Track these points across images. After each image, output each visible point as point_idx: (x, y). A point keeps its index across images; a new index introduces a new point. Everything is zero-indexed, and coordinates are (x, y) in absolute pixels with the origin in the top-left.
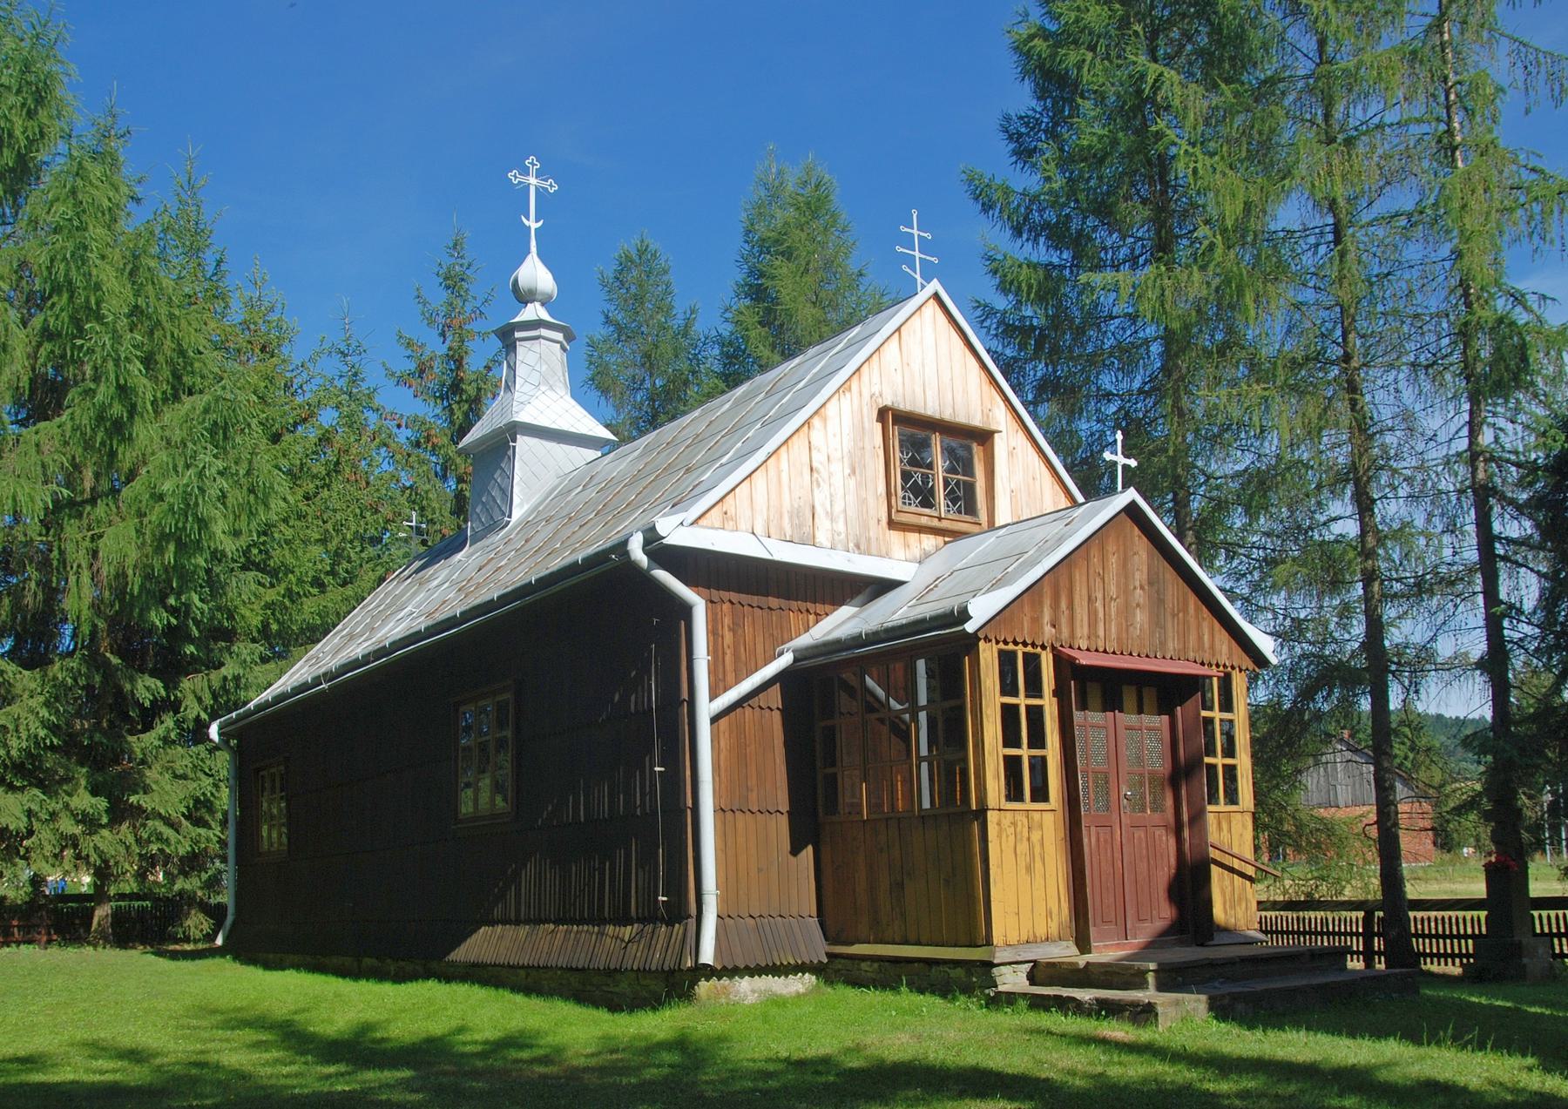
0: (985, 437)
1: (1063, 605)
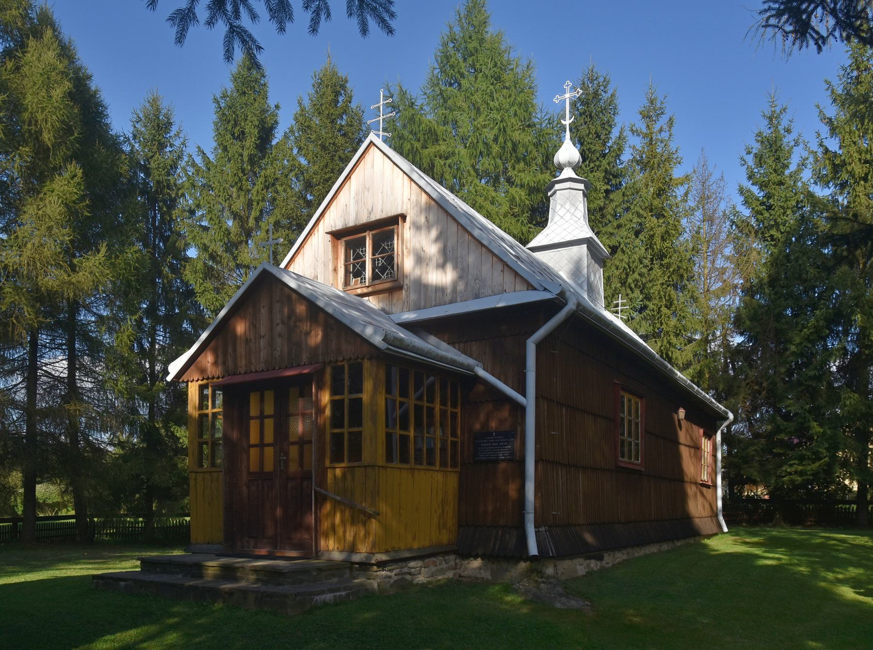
0: (336, 235)
1: (230, 350)
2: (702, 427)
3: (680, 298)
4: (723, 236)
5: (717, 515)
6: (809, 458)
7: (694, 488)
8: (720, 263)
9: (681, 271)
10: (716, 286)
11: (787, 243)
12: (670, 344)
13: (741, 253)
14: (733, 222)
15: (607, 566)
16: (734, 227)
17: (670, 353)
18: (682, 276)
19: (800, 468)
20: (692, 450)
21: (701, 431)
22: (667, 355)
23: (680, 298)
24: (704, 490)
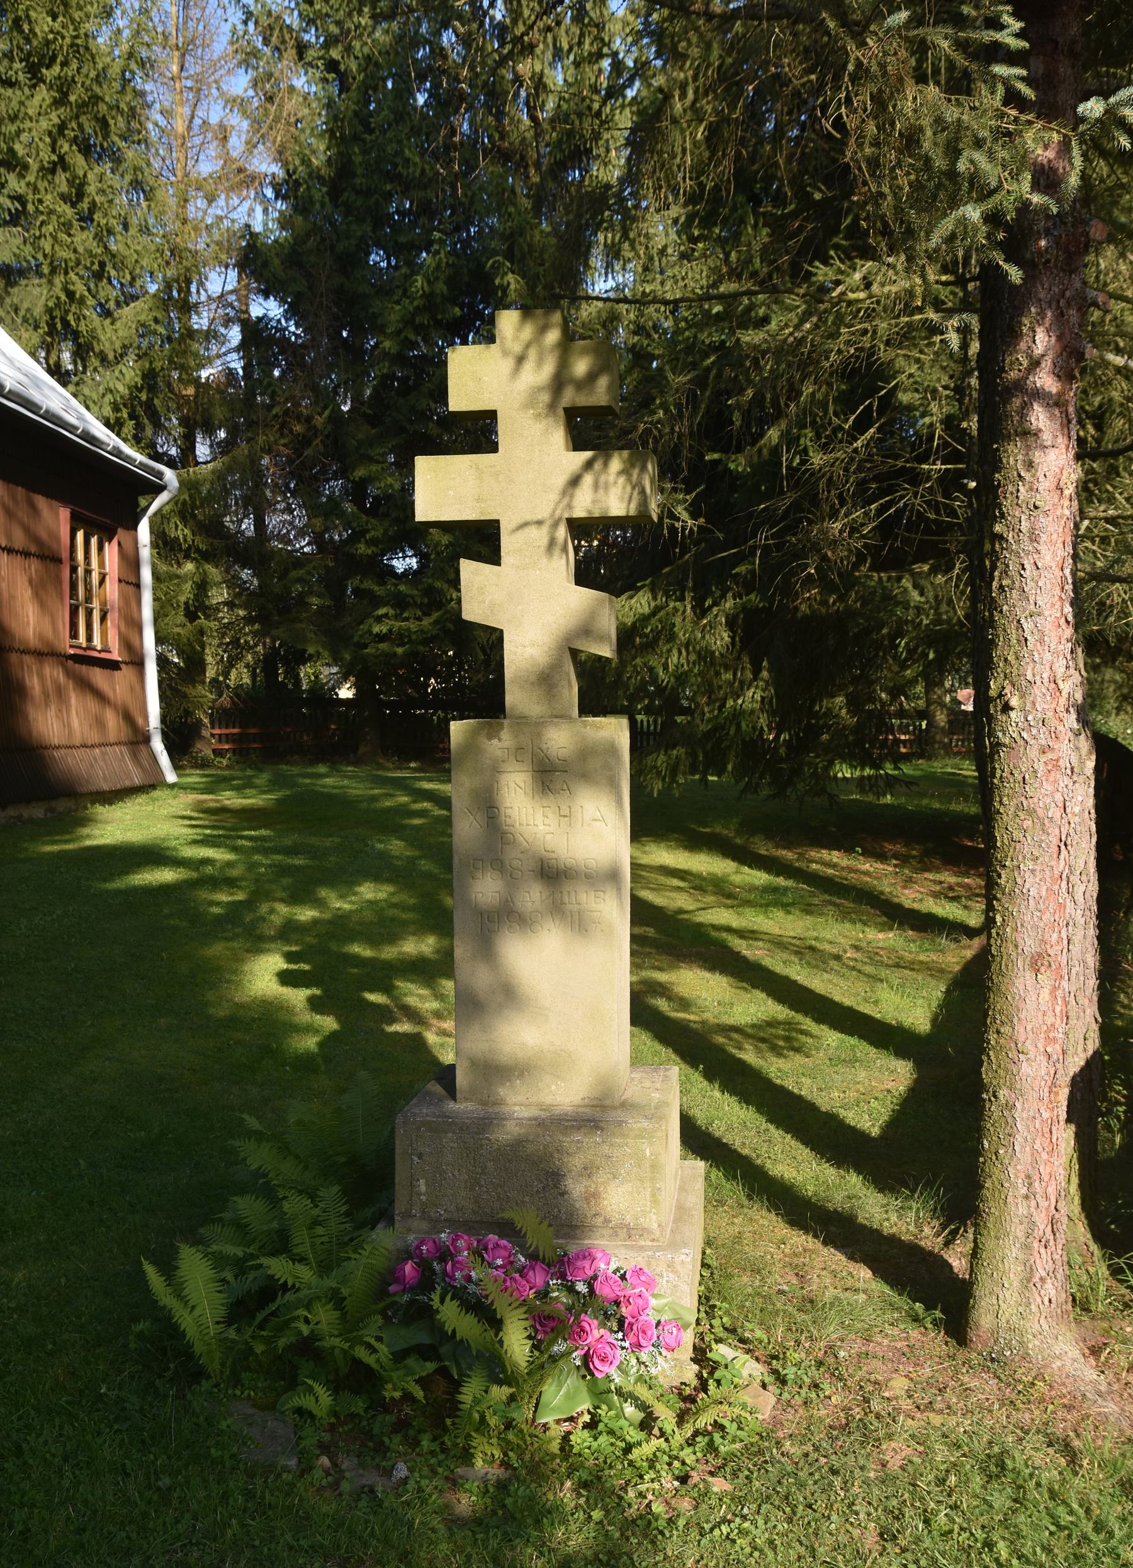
2: (65, 501)
3: (97, 176)
4: (221, 45)
5: (147, 739)
6: (415, 605)
7: (53, 673)
8: (215, 113)
9: (103, 108)
10: (207, 167)
11: (372, 84)
12: (70, 295)
13: (269, 90)
14: (249, 15)
15: (886, 673)
16: (251, 26)
17: (70, 318)
18: (104, 123)
19: (398, 625)
20: (34, 565)
21: (64, 514)
22: (66, 324)
23: (97, 176)
24: (98, 676)
